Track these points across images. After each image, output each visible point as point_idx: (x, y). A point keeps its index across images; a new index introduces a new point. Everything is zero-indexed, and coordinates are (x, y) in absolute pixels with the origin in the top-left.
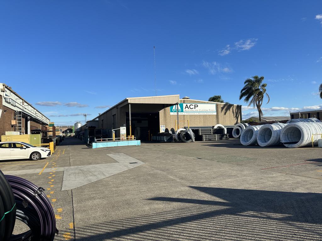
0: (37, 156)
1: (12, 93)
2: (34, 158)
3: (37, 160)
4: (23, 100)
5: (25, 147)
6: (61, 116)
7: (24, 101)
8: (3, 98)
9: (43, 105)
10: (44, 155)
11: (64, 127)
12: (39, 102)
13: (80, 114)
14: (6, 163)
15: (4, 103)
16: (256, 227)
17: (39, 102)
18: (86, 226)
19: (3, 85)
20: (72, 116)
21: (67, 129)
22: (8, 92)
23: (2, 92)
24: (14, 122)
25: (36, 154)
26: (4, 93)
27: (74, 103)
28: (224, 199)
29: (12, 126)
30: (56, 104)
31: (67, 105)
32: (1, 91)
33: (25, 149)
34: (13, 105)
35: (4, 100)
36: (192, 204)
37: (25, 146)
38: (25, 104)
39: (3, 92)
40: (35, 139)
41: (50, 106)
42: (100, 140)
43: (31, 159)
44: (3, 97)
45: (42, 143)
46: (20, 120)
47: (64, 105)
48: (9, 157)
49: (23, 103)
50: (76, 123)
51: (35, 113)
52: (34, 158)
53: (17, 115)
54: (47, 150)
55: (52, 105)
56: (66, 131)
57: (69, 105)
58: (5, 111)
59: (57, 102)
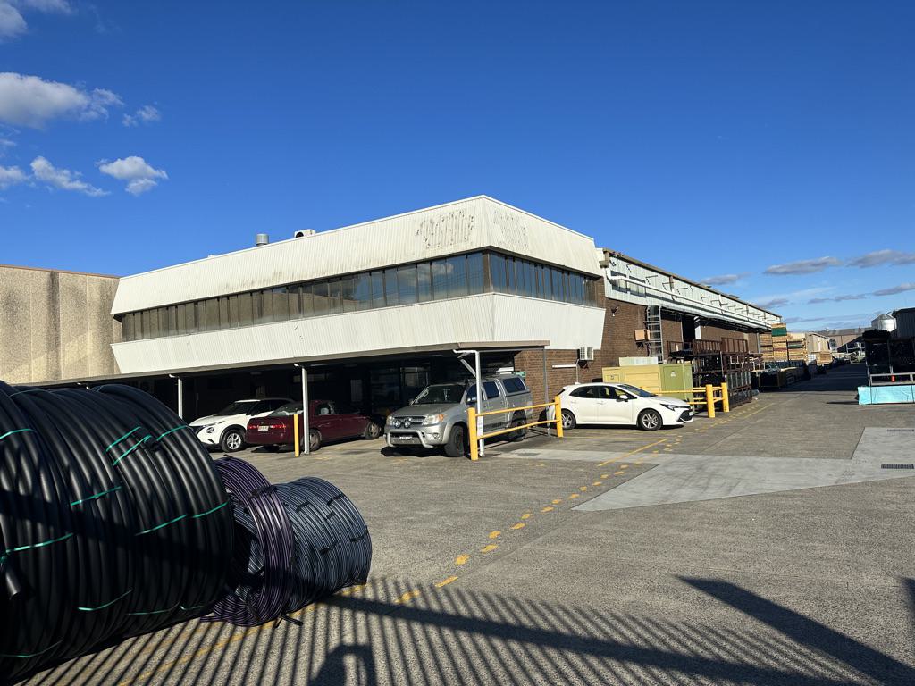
0: (652, 421)
1: (631, 266)
2: (647, 424)
3: (655, 430)
4: (669, 276)
5: (626, 397)
6: (843, 298)
7: (674, 277)
8: (606, 281)
9: (785, 273)
10: (670, 418)
11: (843, 333)
12: (774, 267)
13: (908, 285)
14: (589, 431)
15: (610, 293)
16: (432, 665)
17: (774, 267)
18: (650, 621)
19: (605, 252)
20: (877, 294)
21: (854, 337)
22: (621, 266)
23: (566, 275)
24: (640, 335)
25: (651, 416)
26: (608, 270)
27: (882, 252)
28: (61, 492)
29: (640, 344)
30: (824, 264)
31: (860, 261)
32: (601, 267)
33: (626, 401)
34: (638, 294)
35: (608, 286)
36: (763, 629)
37: (627, 394)
38: (677, 283)
39: (606, 267)
40: (673, 375)
41: (806, 272)
42: (888, 379)
43: (639, 427)
44: (605, 279)
45: (694, 386)
46: (657, 328)
47: (851, 265)
48: (595, 418)
49: (671, 283)
50: (877, 320)
51: (716, 305)
52: (647, 424)
53: (650, 317)
54: (677, 407)
55: (814, 268)
56: (852, 344)
57: (864, 262)
58: (614, 311)
59: (824, 259)
